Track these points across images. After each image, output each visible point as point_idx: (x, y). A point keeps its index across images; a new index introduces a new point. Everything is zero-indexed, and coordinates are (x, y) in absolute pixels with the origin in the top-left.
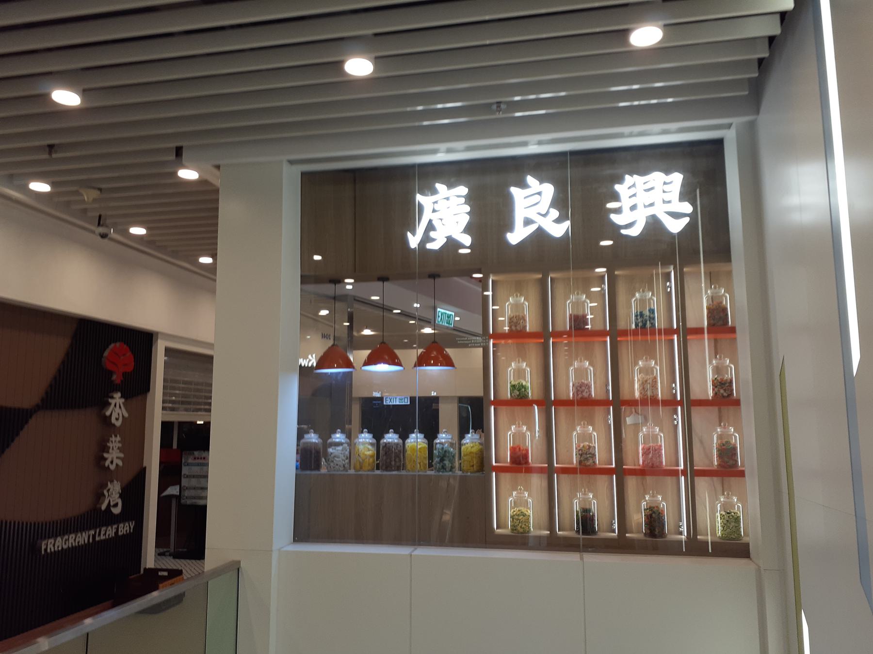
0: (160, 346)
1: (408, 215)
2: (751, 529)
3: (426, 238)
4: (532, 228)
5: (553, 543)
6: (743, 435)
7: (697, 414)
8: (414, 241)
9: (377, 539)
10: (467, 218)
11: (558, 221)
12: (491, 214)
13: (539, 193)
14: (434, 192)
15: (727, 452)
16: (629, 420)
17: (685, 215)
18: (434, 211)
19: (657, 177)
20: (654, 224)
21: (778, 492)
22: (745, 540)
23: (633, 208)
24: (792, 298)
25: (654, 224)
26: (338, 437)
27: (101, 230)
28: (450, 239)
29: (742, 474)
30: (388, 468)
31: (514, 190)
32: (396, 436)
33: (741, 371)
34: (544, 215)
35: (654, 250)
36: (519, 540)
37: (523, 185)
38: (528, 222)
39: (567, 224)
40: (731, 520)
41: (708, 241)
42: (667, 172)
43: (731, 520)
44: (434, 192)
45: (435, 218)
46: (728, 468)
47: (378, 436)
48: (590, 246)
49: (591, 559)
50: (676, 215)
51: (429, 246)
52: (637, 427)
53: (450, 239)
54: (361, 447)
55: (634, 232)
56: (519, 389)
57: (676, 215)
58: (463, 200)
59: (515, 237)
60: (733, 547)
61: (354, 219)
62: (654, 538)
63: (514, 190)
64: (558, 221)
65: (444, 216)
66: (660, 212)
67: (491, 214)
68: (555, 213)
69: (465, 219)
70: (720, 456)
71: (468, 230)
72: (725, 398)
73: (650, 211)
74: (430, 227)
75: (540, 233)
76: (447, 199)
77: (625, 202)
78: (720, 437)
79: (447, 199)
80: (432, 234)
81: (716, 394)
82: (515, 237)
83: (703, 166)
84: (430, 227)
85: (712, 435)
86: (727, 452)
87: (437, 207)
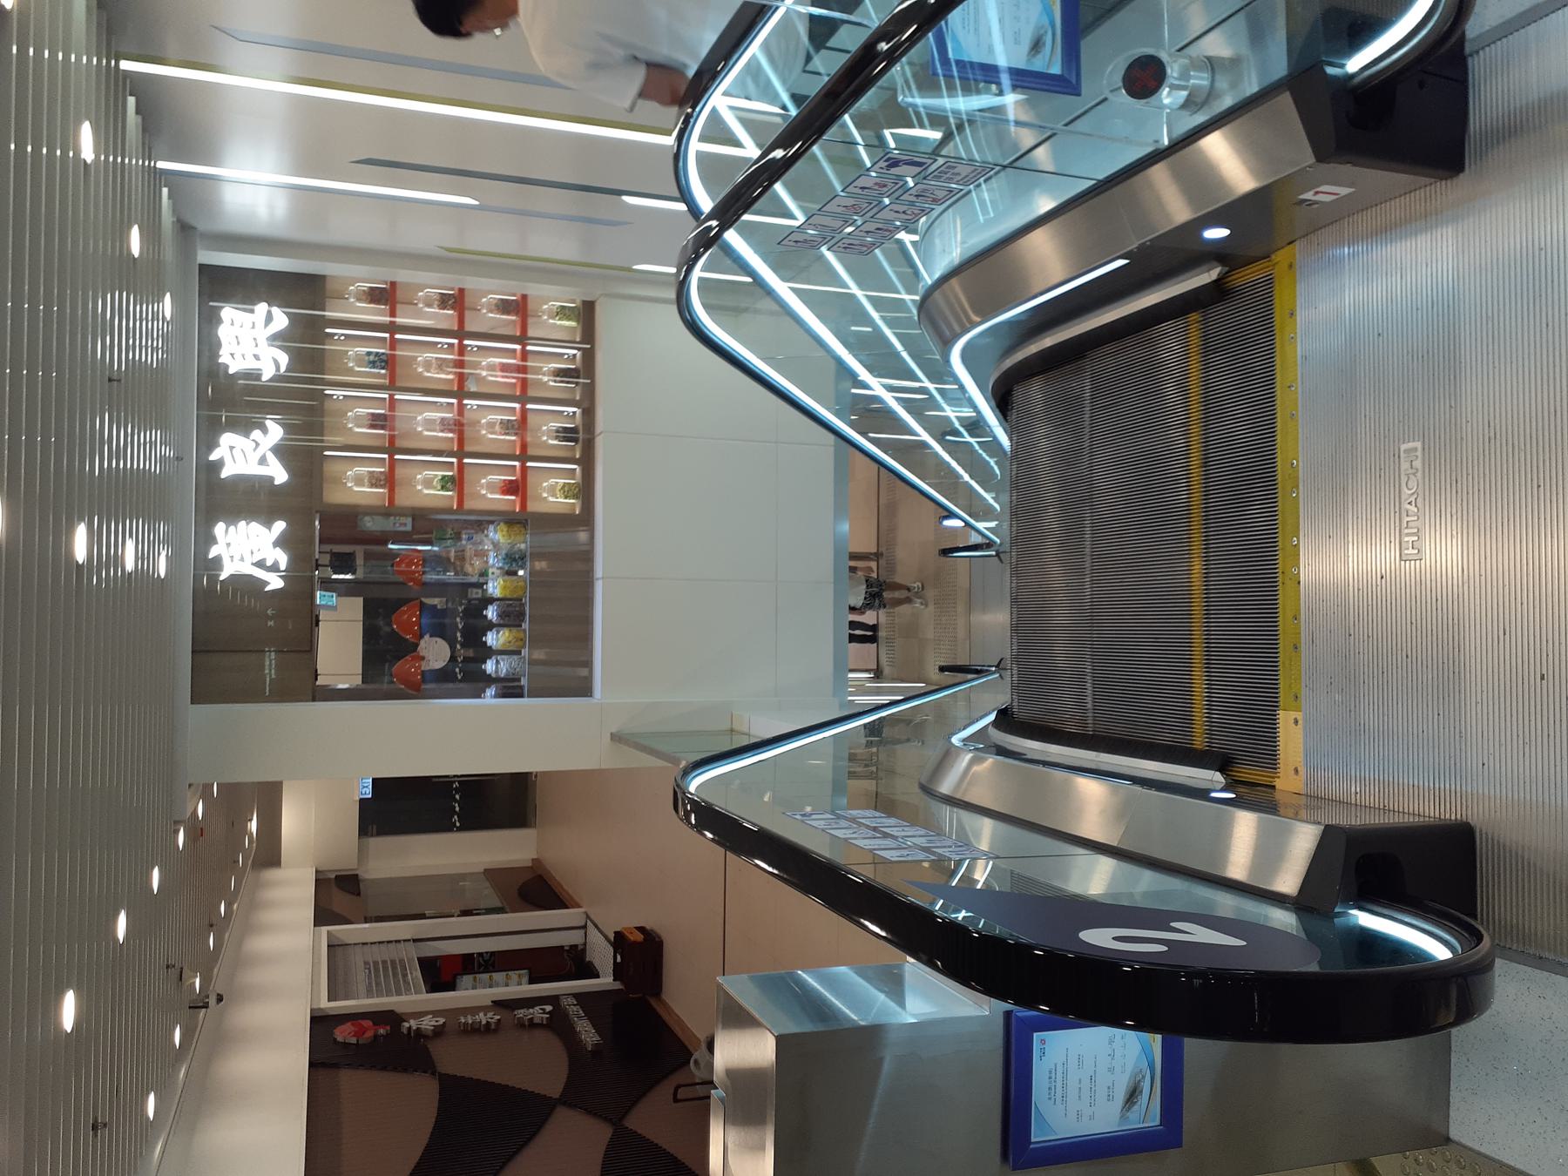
0: (324, 1004)
1: (246, 586)
2: (569, 296)
3: (274, 568)
4: (271, 458)
5: (587, 462)
6: (489, 291)
7: (469, 327)
8: (275, 582)
9: (587, 621)
10: (254, 524)
11: (265, 430)
12: (249, 500)
13: (232, 448)
14: (218, 560)
15: (504, 307)
16: (473, 389)
17: (269, 313)
18: (242, 559)
19: (224, 332)
20: (278, 339)
21: (527, 269)
22: (579, 302)
23: (257, 357)
24: (344, 230)
25: (278, 339)
26: (490, 667)
27: (212, 1001)
28: (277, 544)
29: (524, 297)
30: (521, 615)
31: (224, 475)
32: (490, 608)
33: (431, 284)
34: (257, 444)
35: (308, 343)
36: (585, 491)
37: (219, 464)
38: (263, 461)
39: (269, 423)
40: (563, 312)
41: (301, 292)
42: (219, 321)
43: (563, 312)
44: (218, 560)
45: (249, 560)
46: (385, 296)
47: (491, 626)
48: (301, 402)
49: (600, 425)
50: (269, 318)
51: (283, 567)
52: (479, 379)
53: (277, 544)
54: (501, 641)
55: (284, 359)
56: (445, 483)
57: (269, 318)
58: (232, 528)
59: (280, 475)
60: (586, 314)
61: (246, 648)
62: (583, 373)
63: (224, 475)
64: (265, 430)
65: (250, 550)
66: (264, 333)
67: (249, 500)
68: (256, 434)
69: (255, 527)
70: (508, 313)
71: (268, 524)
72: (457, 301)
73: (263, 342)
74: (260, 564)
75: (278, 450)
76: (228, 545)
77: (250, 364)
78: (359, 300)
79: (228, 545)
80: (269, 563)
81: (453, 308)
82: (280, 475)
83: (227, 285)
84: (260, 564)
85: (487, 317)
86: (504, 307)
87: (237, 557)
